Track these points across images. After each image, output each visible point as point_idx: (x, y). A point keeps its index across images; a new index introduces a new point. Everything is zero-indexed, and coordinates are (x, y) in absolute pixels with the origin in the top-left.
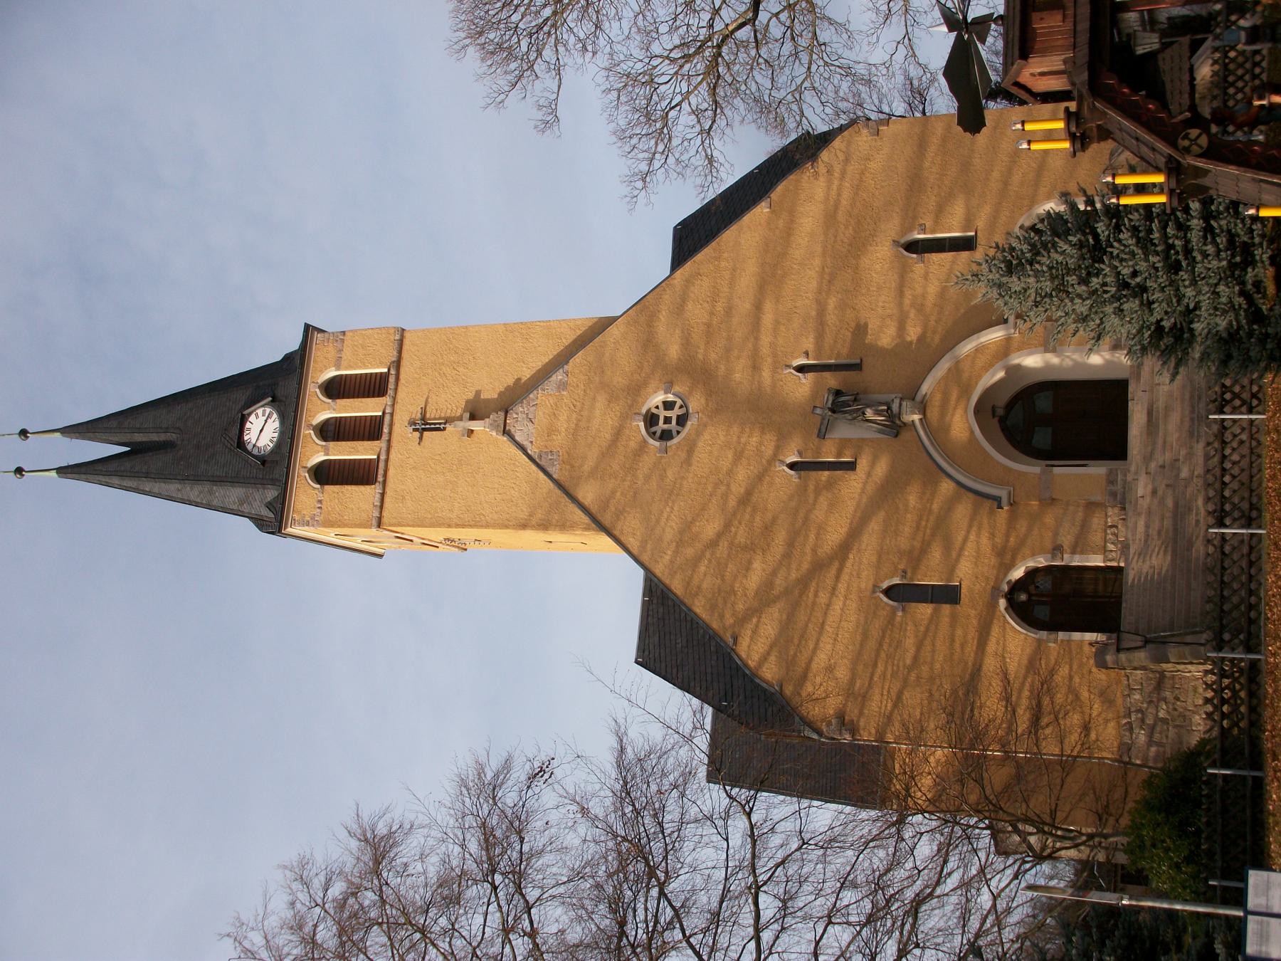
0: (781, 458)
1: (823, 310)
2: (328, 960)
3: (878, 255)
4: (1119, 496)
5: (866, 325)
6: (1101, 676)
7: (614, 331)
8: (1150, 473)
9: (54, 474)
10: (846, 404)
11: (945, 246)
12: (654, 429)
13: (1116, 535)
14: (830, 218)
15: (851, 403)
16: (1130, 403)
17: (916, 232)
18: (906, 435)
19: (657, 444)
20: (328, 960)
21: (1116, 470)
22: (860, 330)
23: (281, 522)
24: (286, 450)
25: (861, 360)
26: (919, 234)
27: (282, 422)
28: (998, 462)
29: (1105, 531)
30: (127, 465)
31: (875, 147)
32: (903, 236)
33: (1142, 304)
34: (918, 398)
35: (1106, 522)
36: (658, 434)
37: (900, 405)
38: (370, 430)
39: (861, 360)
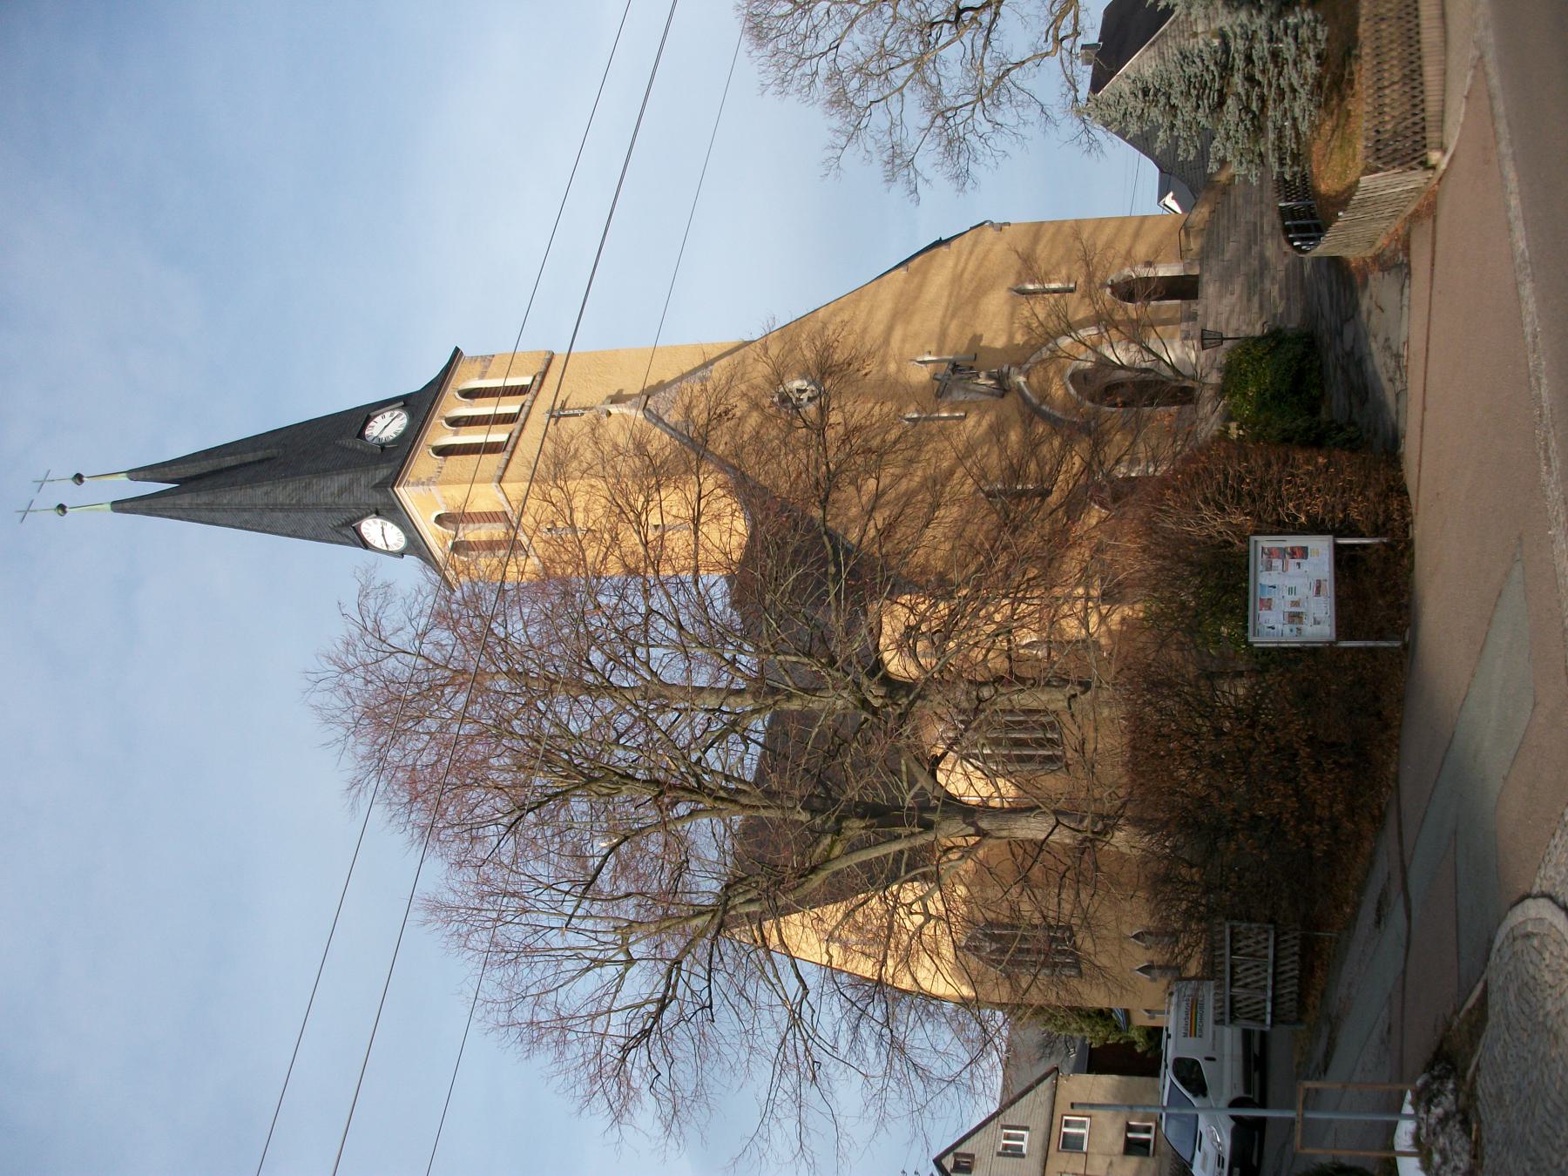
5: (981, 336)
6: (1171, 91)
7: (752, 346)
9: (123, 478)
14: (957, 279)
22: (977, 338)
23: (396, 479)
27: (409, 421)
30: (169, 501)
31: (832, 662)
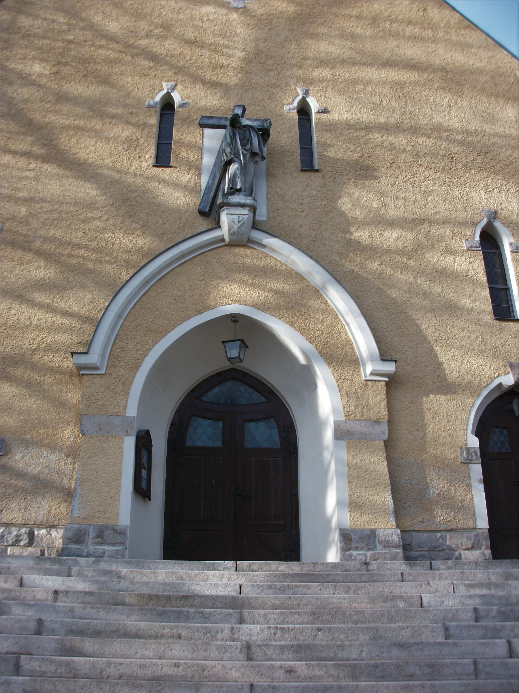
0: (179, 87)
1: (387, 130)
3: (474, 194)
4: (75, 546)
8: (56, 599)
10: (246, 141)
11: (497, 283)
13: (16, 543)
15: (248, 147)
16: (229, 564)
17: (512, 241)
18: (202, 224)
21: (123, 543)
25: (317, 171)
26: (511, 244)
28: (149, 350)
29: (25, 525)
32: (504, 224)
34: (257, 235)
35: (40, 526)
37: (243, 206)
39: (317, 171)
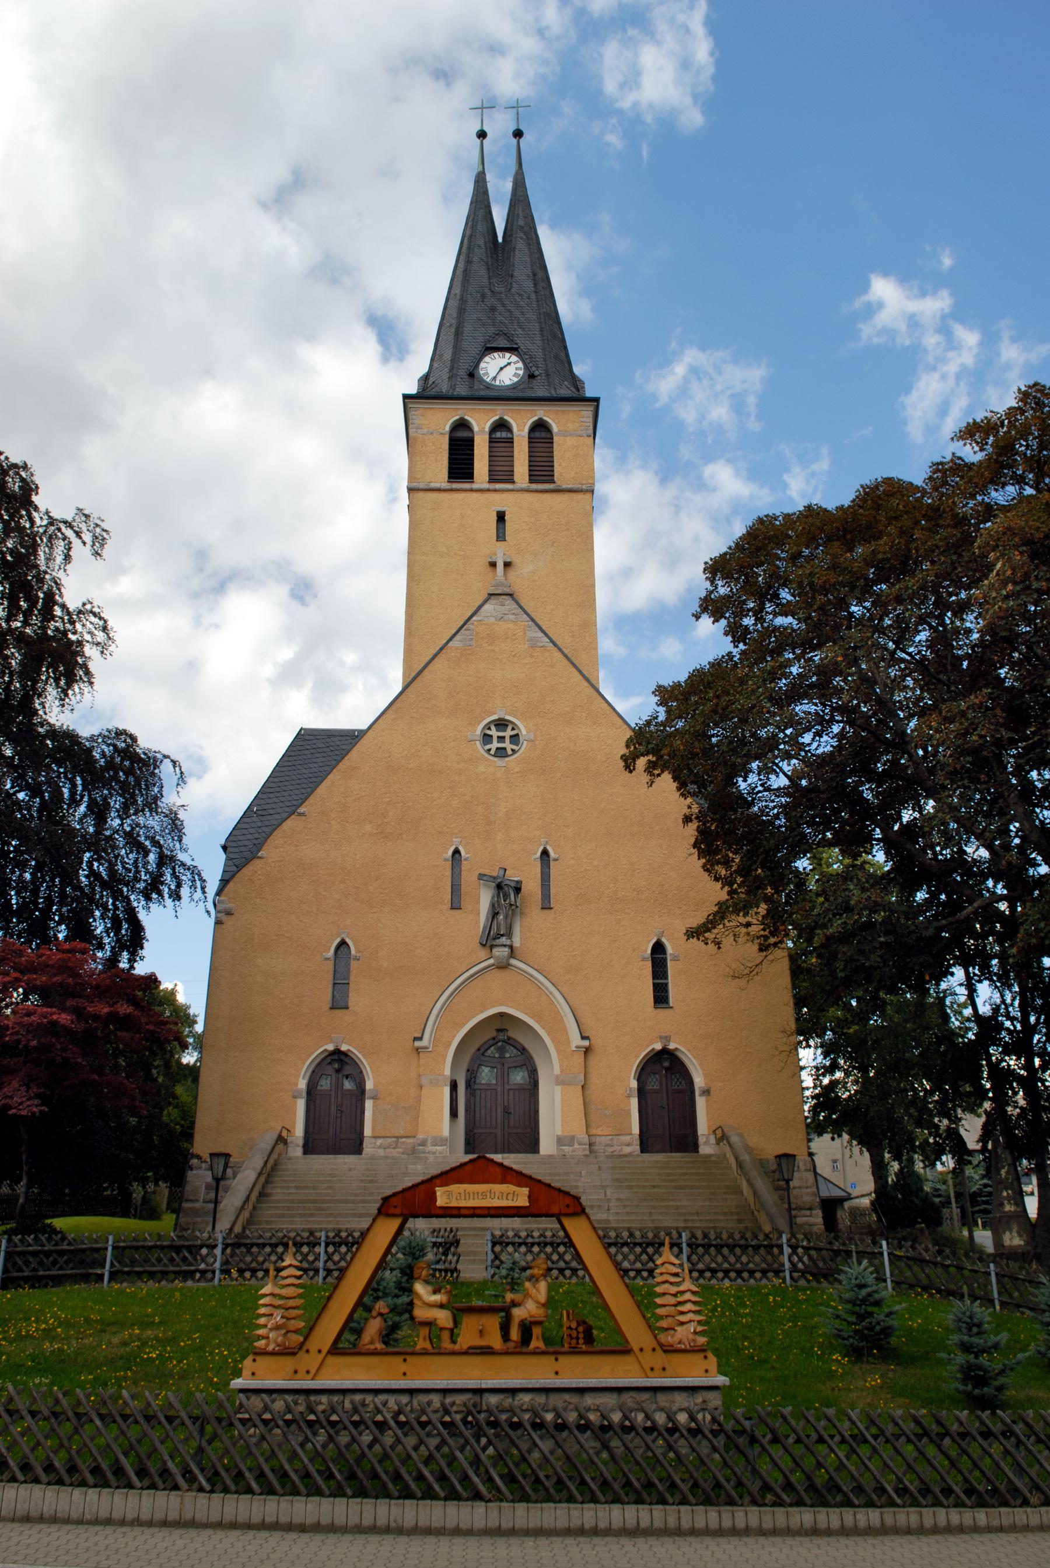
2: (5, 1431)
12: (493, 727)
19: (478, 732)
20: (5, 1431)
24: (520, 177)
33: (704, 722)
36: (488, 732)
37: (505, 946)
38: (502, 474)
